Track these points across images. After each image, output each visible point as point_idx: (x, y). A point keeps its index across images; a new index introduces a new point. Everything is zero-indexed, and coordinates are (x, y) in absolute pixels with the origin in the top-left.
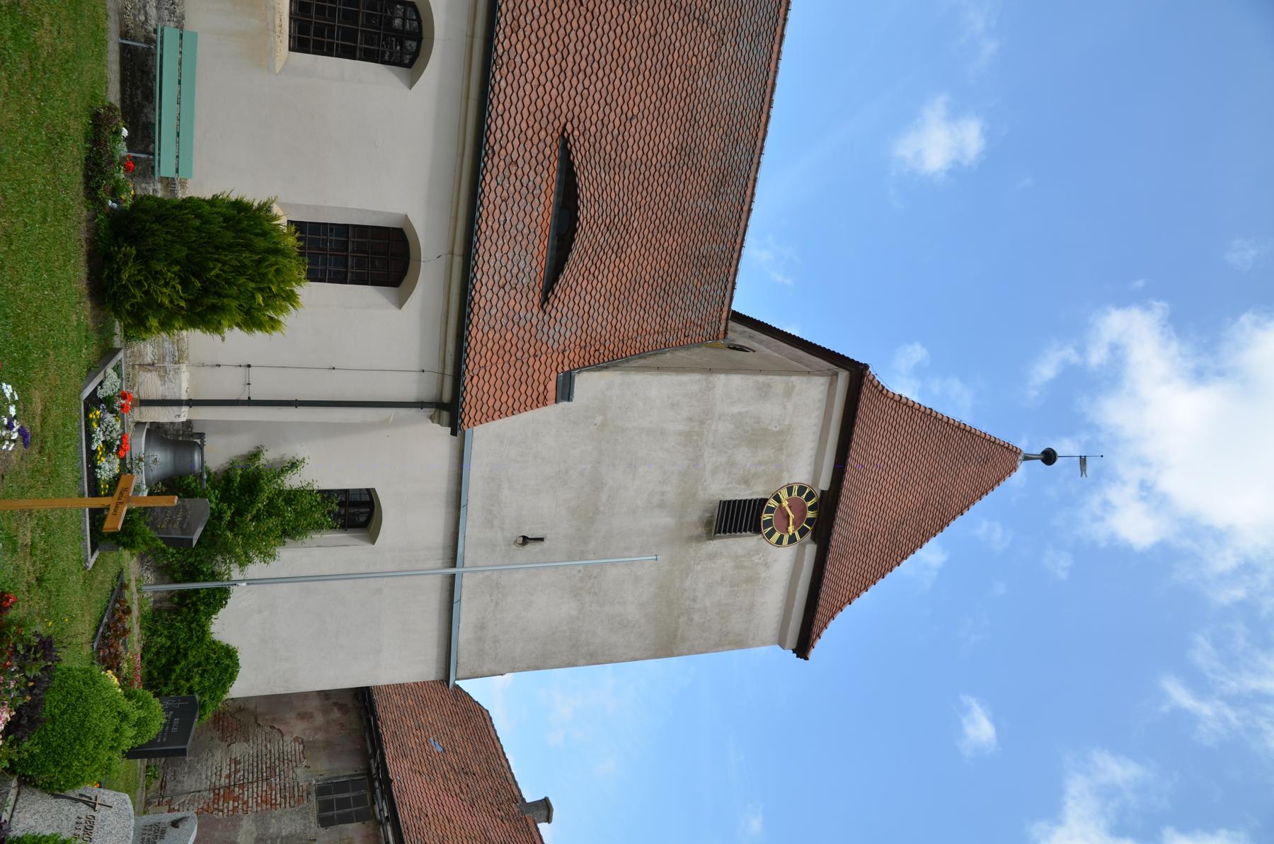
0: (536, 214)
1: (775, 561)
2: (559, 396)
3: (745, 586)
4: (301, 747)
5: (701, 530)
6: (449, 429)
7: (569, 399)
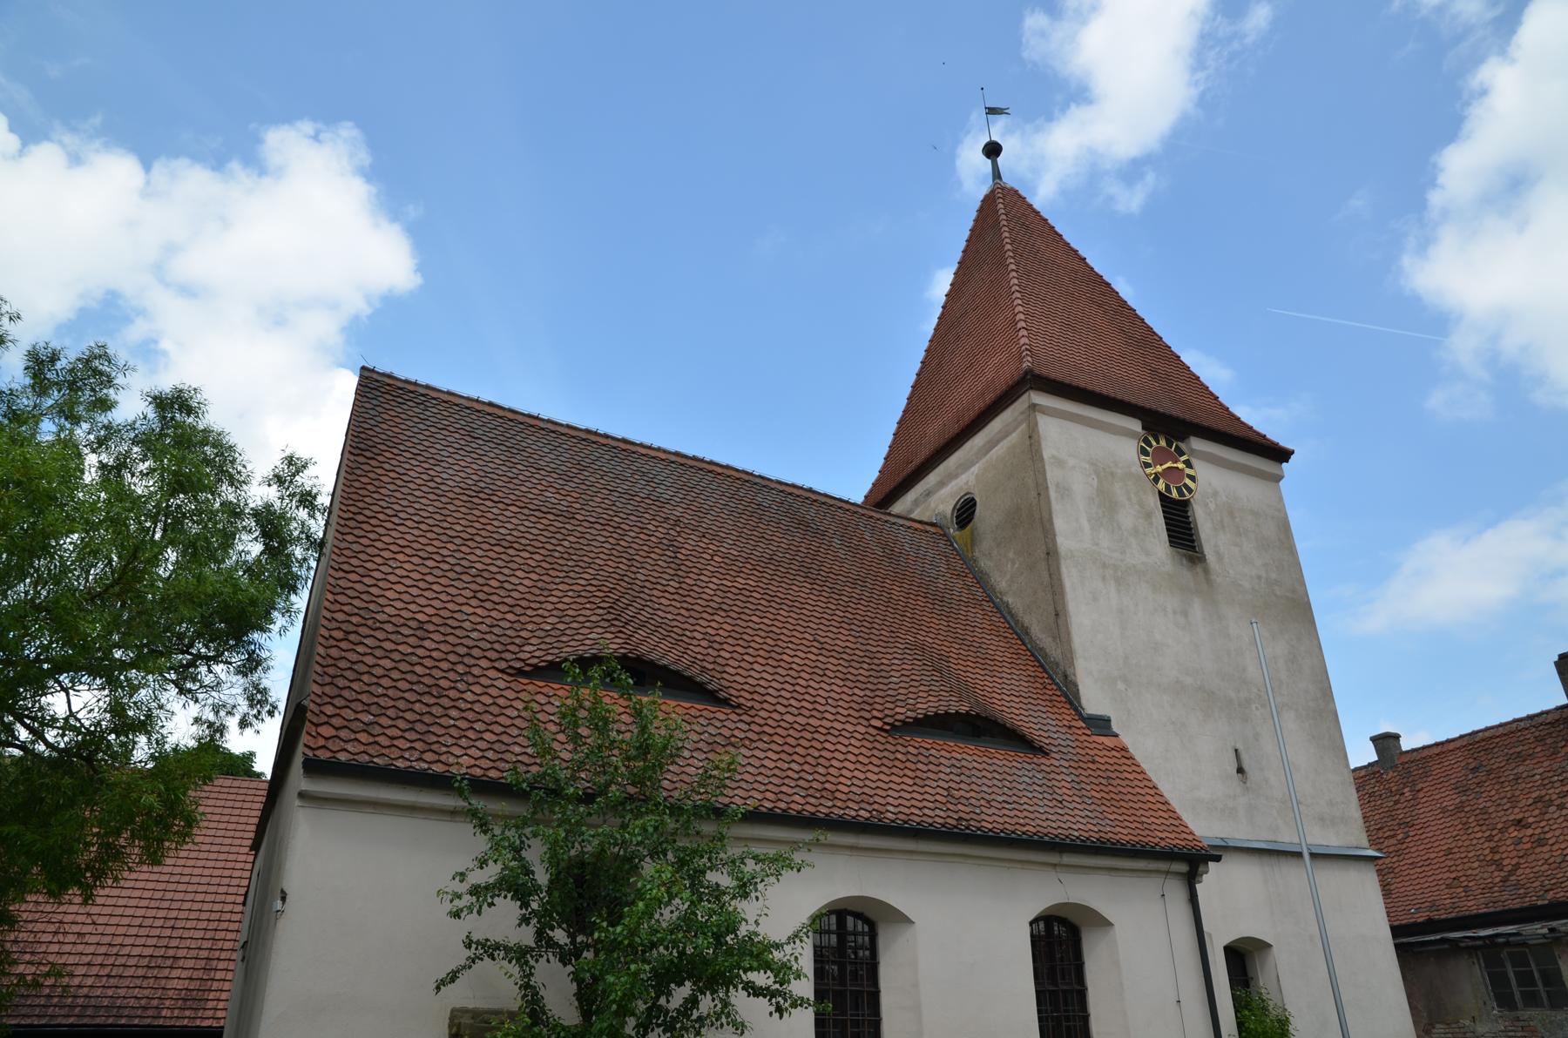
0: (543, 702)
1: (1210, 484)
2: (1104, 732)
3: (1237, 520)
4: (1438, 1026)
5: (1199, 569)
6: (1211, 864)
7: (1108, 720)
